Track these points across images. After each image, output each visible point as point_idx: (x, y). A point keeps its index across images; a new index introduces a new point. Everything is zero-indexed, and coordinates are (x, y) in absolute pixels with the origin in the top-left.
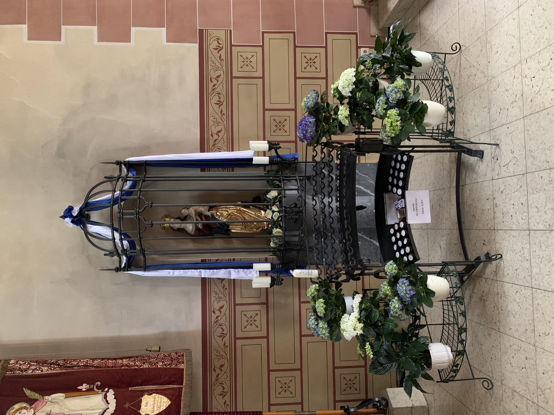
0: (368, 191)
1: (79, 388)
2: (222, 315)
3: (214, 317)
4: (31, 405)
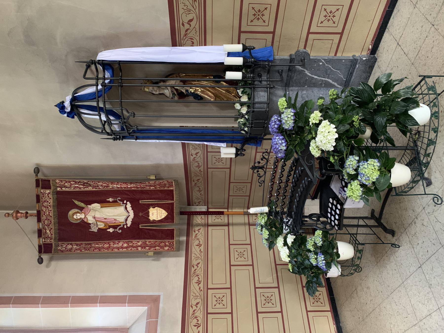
0: (336, 84)
2: (198, 157)
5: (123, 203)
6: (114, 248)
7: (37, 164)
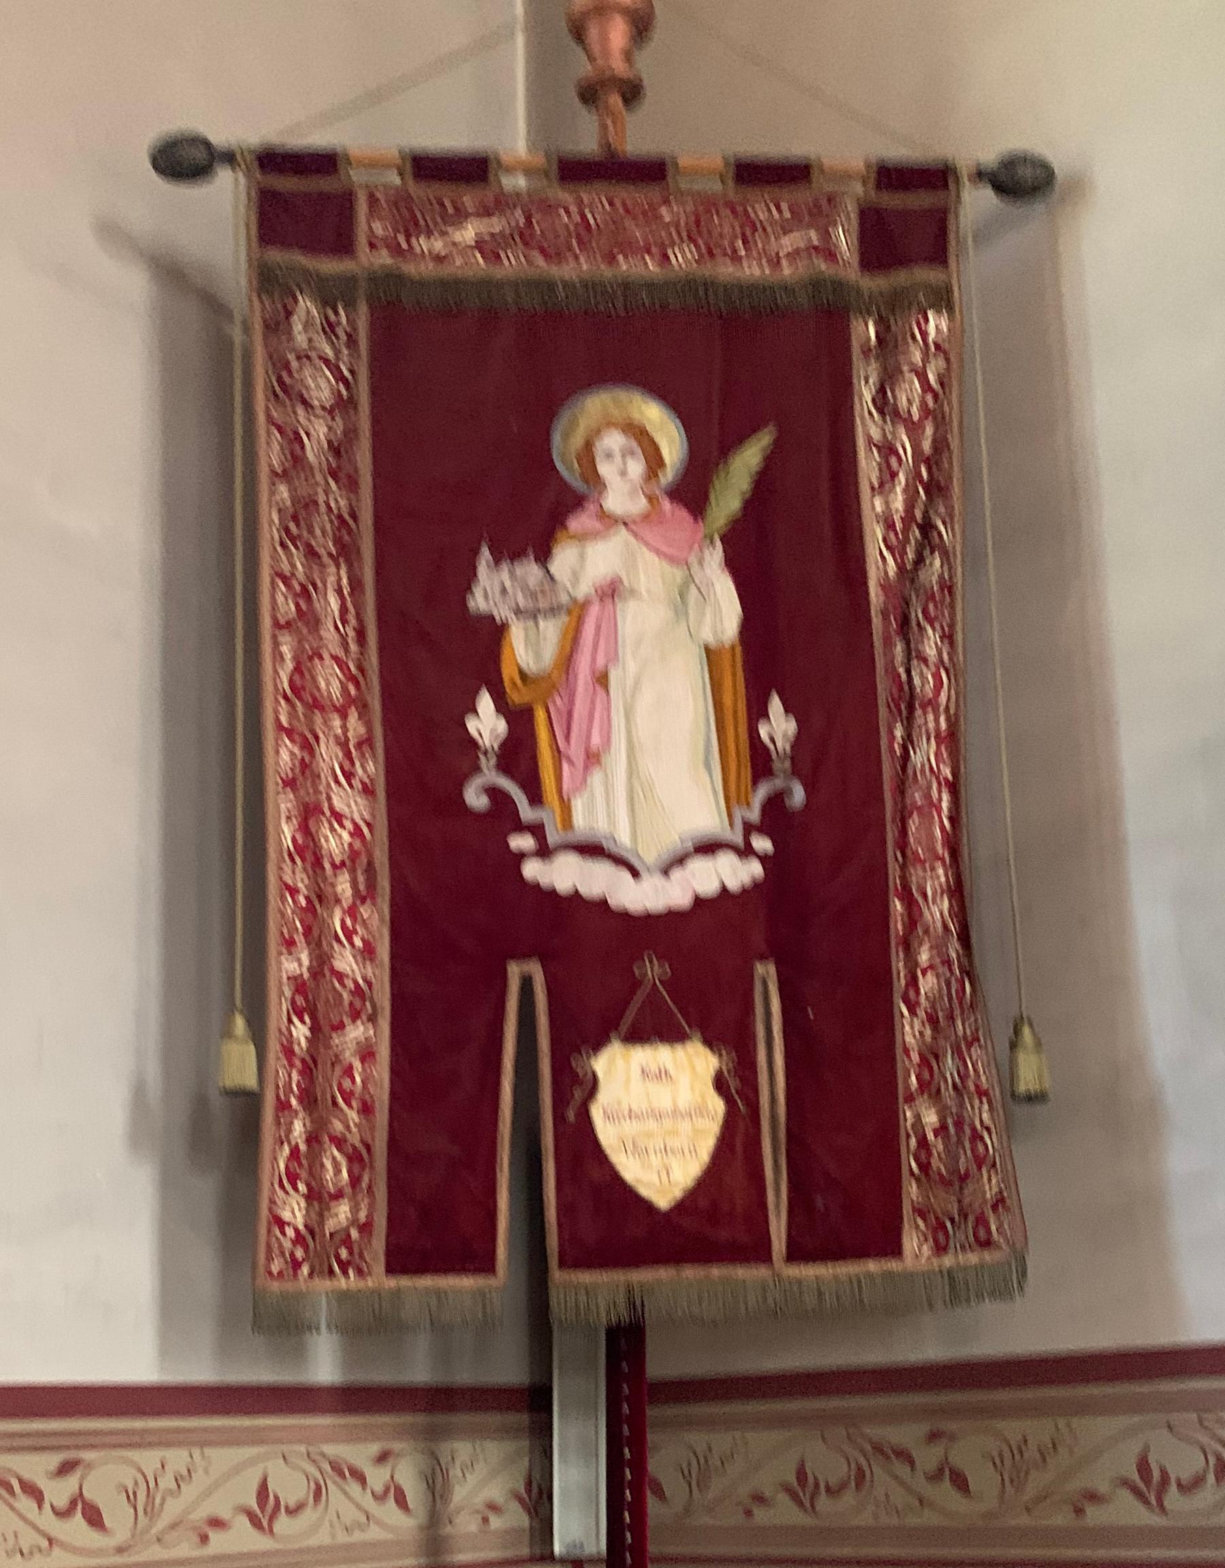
1: (776, 705)
3: (906, 1435)
4: (677, 493)
5: (748, 829)
6: (308, 747)
7: (1079, 187)
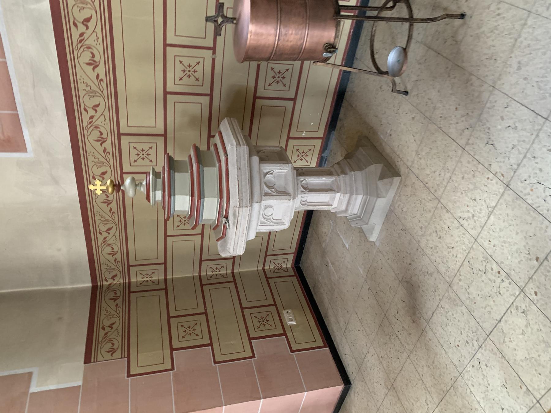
3: (100, 238)
